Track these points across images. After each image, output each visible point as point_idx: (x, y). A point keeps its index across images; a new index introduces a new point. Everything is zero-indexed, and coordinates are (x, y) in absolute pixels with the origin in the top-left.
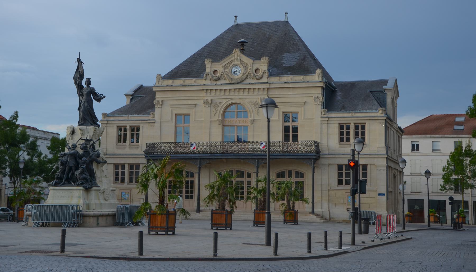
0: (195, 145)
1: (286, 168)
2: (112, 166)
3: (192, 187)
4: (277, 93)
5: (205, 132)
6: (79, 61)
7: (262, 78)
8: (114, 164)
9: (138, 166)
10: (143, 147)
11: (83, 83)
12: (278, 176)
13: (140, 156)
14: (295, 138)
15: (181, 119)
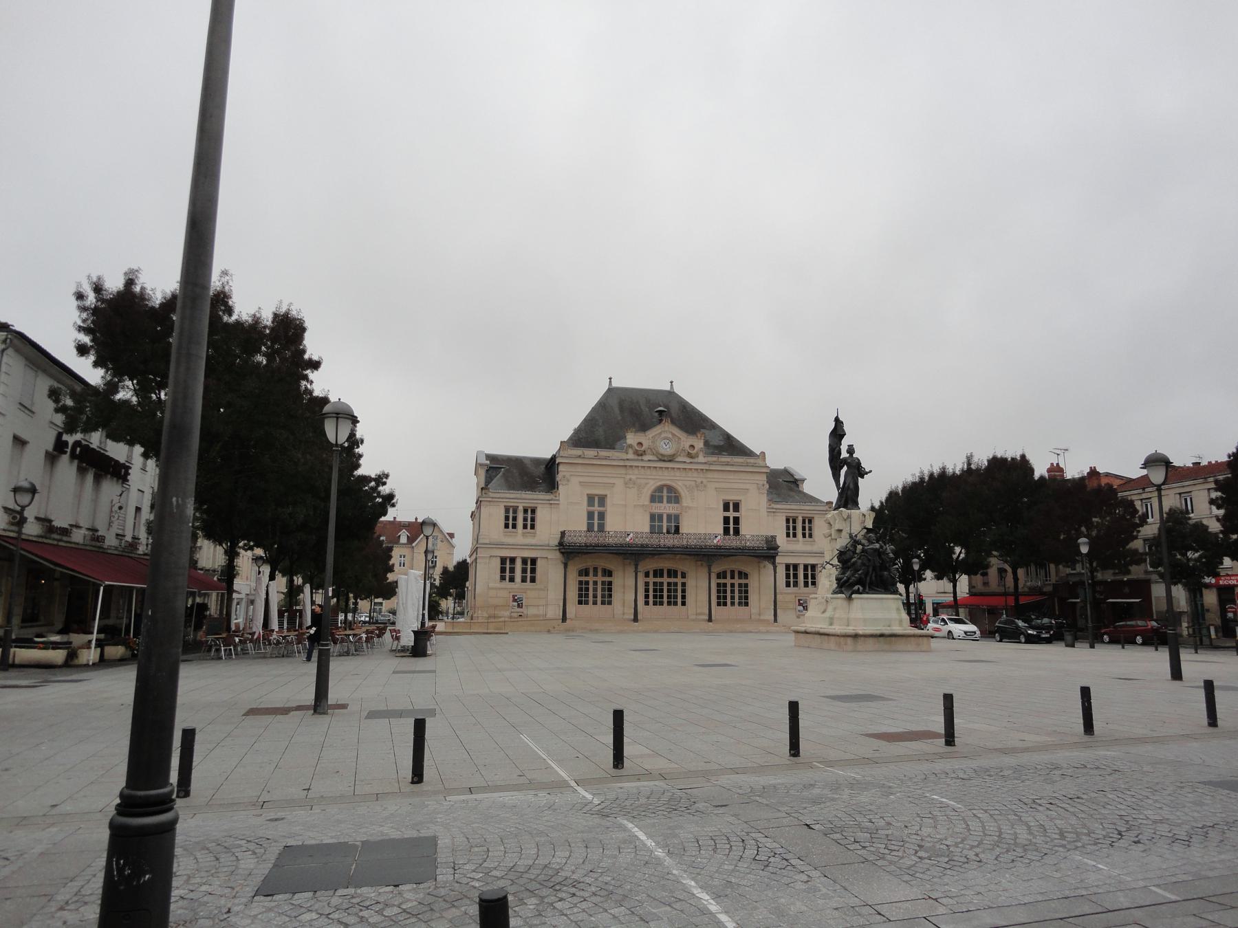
1: (589, 563)
2: (499, 561)
3: (719, 597)
5: (629, 521)
6: (837, 420)
11: (844, 448)
12: (719, 576)
14: (737, 532)
15: (597, 501)
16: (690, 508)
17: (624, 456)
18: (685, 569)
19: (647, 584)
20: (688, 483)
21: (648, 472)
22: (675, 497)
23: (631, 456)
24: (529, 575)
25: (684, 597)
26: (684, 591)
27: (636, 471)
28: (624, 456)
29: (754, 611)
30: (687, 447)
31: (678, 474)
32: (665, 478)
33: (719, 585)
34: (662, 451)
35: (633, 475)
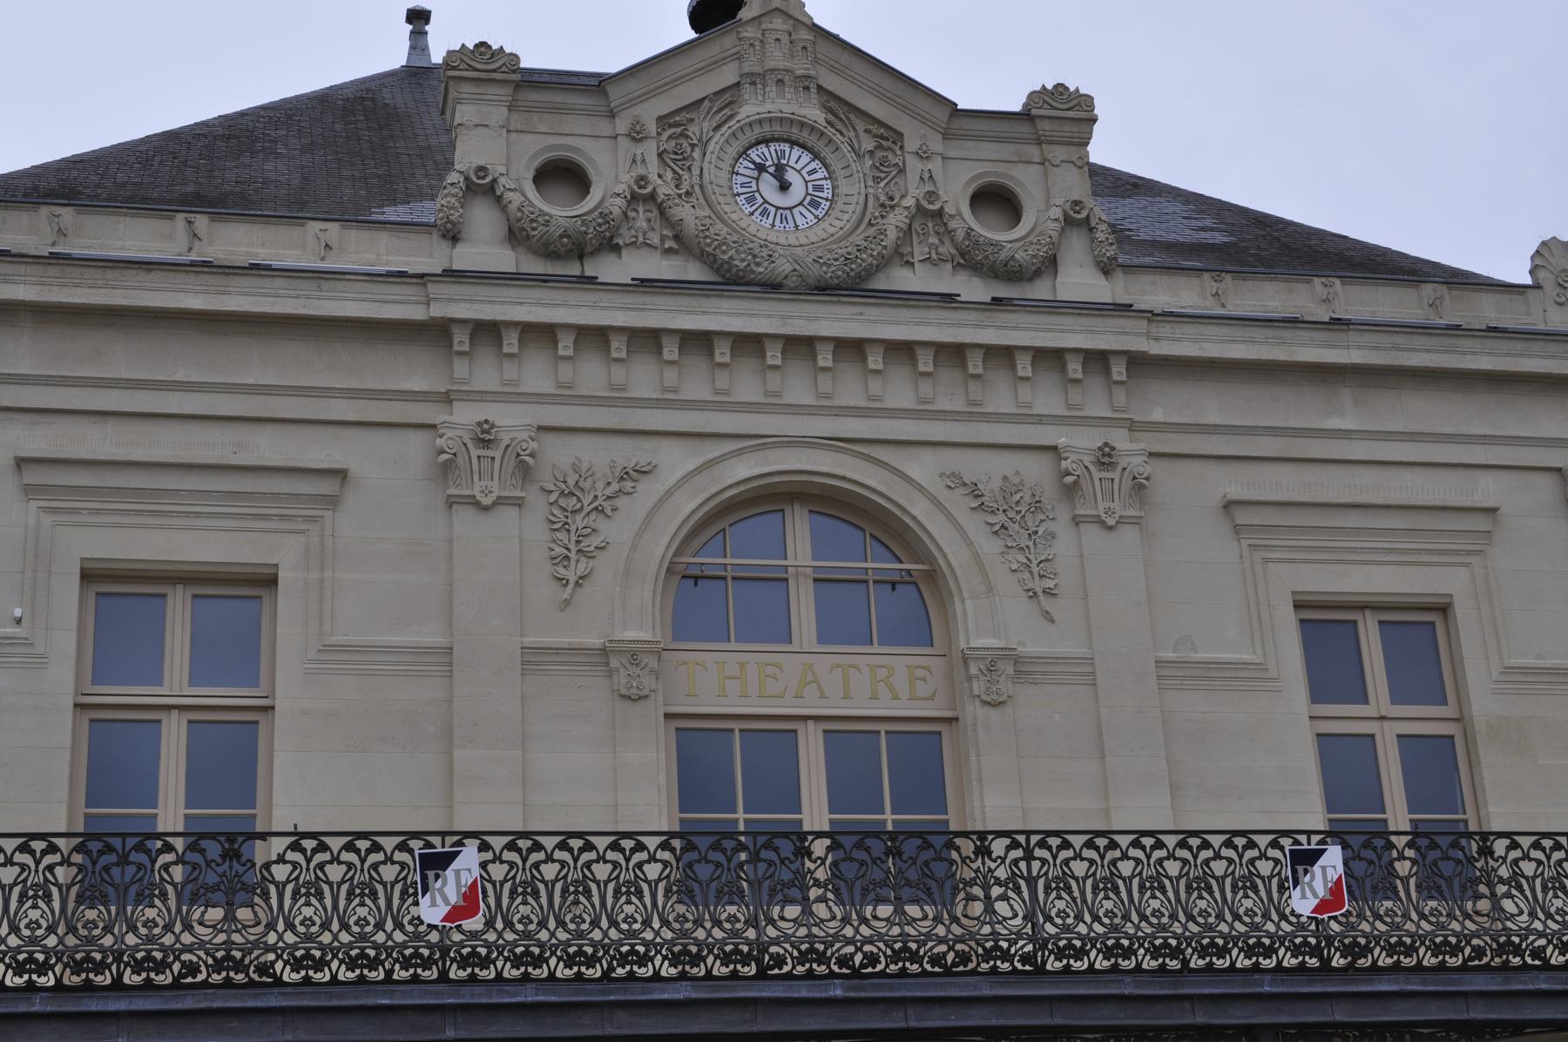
0: (469, 860)
4: (1213, 418)
7: (1050, 264)
16: (1024, 667)
17: (424, 256)
20: (989, 469)
22: (890, 573)
23: (483, 248)
27: (536, 374)
28: (424, 256)
30: (955, 195)
31: (899, 390)
32: (797, 424)
35: (511, 398)
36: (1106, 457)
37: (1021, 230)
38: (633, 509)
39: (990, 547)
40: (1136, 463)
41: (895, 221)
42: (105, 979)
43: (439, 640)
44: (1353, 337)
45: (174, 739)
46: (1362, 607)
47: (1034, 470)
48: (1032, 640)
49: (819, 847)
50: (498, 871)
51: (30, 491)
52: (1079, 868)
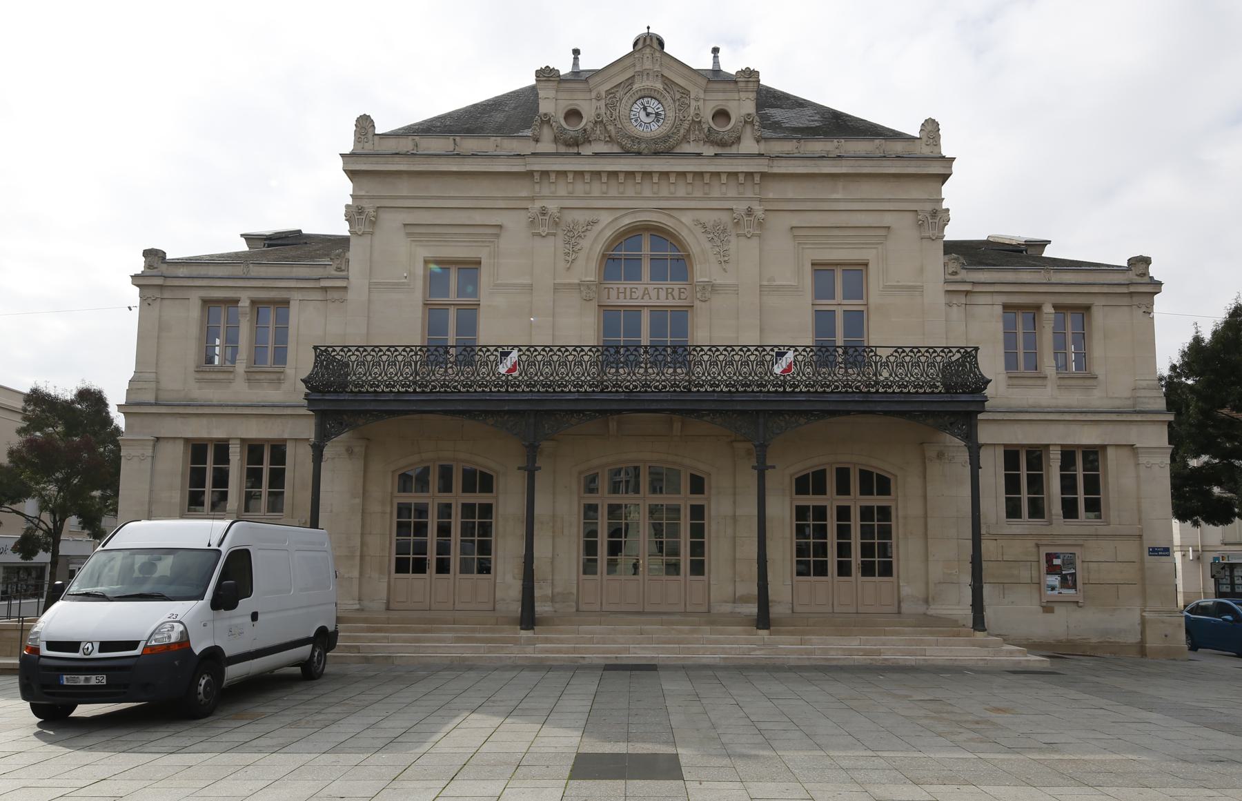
0: (790, 355)
2: (179, 448)
4: (790, 196)
7: (738, 140)
8: (187, 440)
9: (278, 451)
10: (301, 363)
13: (289, 411)
16: (713, 288)
18: (701, 468)
19: (590, 510)
20: (709, 218)
21: (596, 188)
22: (673, 259)
23: (546, 146)
24: (1024, 496)
25: (698, 548)
26: (698, 531)
27: (562, 190)
29: (906, 590)
30: (707, 114)
31: (681, 191)
32: (644, 204)
33: (801, 512)
34: (639, 131)
35: (553, 198)
36: (749, 212)
37: (729, 127)
38: (591, 235)
39: (708, 246)
40: (760, 214)
41: (686, 125)
42: (503, 390)
43: (529, 282)
44: (844, 162)
45: (452, 313)
46: (837, 264)
47: (725, 217)
48: (719, 280)
49: (452, 351)
50: (524, 358)
51: (408, 234)
52: (923, 359)
